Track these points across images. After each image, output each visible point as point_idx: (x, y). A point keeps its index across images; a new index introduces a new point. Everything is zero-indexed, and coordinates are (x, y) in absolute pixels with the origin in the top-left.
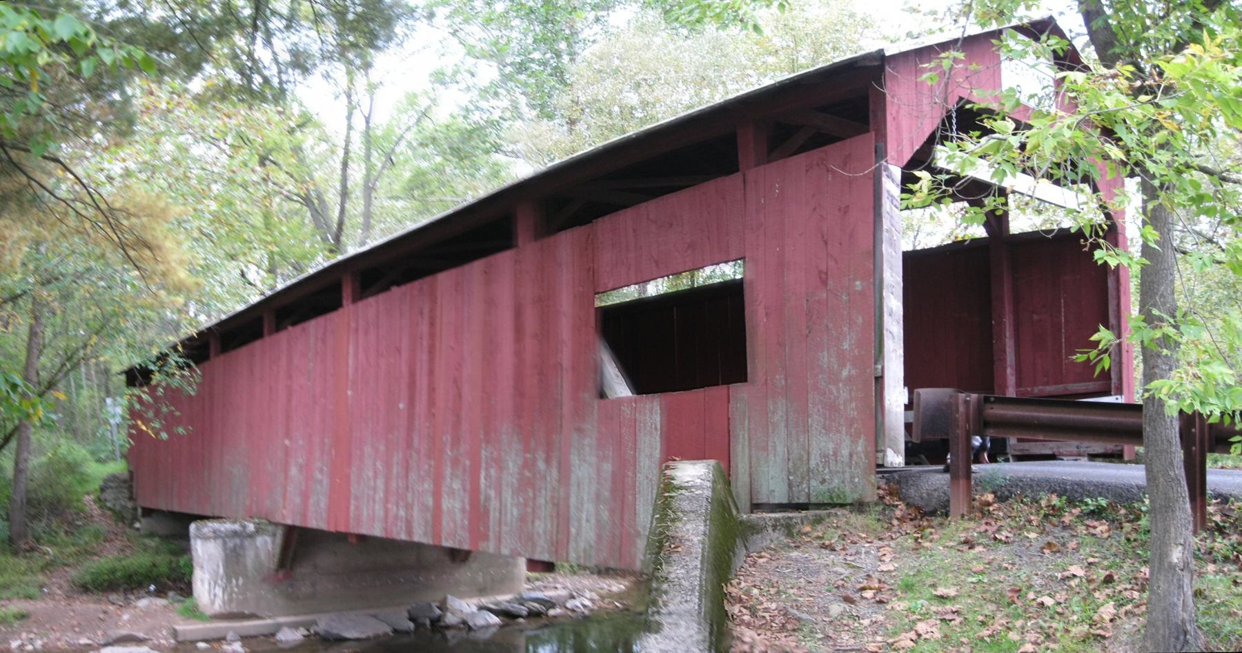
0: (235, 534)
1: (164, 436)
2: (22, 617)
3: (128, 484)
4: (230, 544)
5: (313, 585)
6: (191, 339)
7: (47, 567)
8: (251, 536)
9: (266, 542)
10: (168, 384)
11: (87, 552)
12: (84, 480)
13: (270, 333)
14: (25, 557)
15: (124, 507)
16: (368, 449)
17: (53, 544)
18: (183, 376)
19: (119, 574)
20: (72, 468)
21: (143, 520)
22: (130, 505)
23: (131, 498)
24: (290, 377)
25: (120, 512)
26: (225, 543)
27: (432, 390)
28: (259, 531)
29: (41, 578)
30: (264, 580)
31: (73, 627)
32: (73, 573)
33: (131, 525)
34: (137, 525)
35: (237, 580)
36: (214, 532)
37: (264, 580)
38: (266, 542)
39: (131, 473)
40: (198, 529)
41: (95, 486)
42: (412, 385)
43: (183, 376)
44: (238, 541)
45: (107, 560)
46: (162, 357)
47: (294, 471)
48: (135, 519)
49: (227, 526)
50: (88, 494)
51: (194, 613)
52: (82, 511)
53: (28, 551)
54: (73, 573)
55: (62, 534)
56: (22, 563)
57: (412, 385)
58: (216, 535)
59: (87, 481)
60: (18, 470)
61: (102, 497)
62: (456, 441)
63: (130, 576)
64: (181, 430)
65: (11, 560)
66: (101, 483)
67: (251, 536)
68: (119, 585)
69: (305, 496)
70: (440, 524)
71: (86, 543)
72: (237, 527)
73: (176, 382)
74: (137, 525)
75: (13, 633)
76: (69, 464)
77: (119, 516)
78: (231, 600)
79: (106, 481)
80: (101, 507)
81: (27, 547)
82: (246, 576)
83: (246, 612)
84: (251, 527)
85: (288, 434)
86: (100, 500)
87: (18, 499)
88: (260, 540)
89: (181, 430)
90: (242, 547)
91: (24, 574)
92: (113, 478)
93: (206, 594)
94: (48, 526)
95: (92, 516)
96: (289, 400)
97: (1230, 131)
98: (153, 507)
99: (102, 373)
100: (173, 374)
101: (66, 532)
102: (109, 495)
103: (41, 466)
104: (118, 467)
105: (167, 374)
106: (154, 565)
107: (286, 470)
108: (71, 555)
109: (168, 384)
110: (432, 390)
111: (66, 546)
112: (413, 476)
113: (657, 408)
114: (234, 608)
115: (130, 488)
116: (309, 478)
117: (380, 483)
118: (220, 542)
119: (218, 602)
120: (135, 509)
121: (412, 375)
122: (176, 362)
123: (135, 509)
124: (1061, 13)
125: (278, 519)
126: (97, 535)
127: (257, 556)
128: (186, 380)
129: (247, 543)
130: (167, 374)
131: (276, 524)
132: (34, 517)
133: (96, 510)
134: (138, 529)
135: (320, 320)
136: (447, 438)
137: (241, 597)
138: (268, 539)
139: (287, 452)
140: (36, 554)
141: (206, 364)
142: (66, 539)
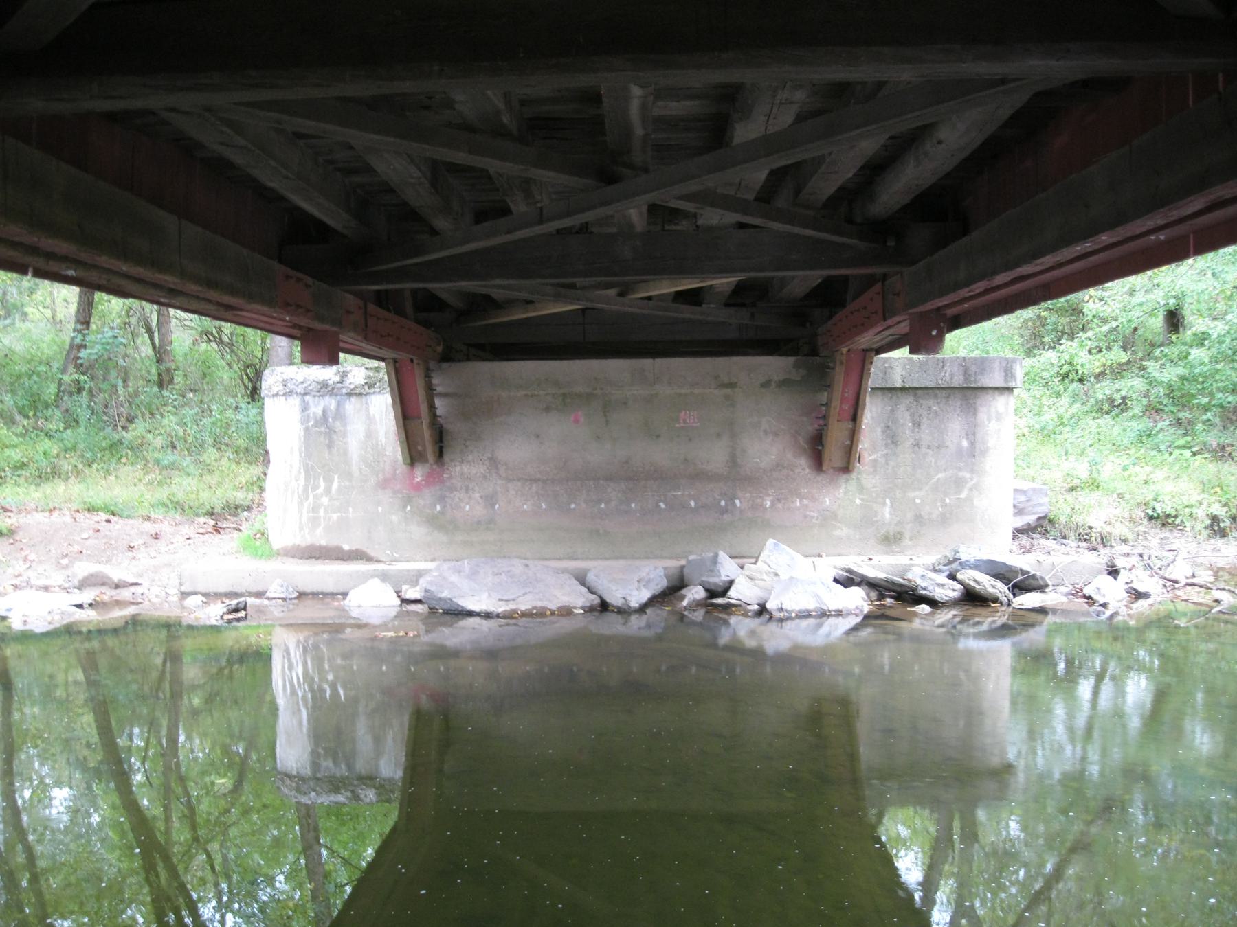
4: (317, 407)
5: (490, 500)
26: (305, 408)
30: (384, 484)
35: (329, 481)
37: (384, 484)
44: (331, 402)
51: (260, 543)
70: (1090, 256)
78: (314, 521)
82: (348, 475)
83: (346, 547)
90: (340, 414)
97: (125, 594)
99: (15, 306)
113: (384, 773)
114: (321, 539)
124: (938, 924)
129: (351, 406)
137: (335, 516)
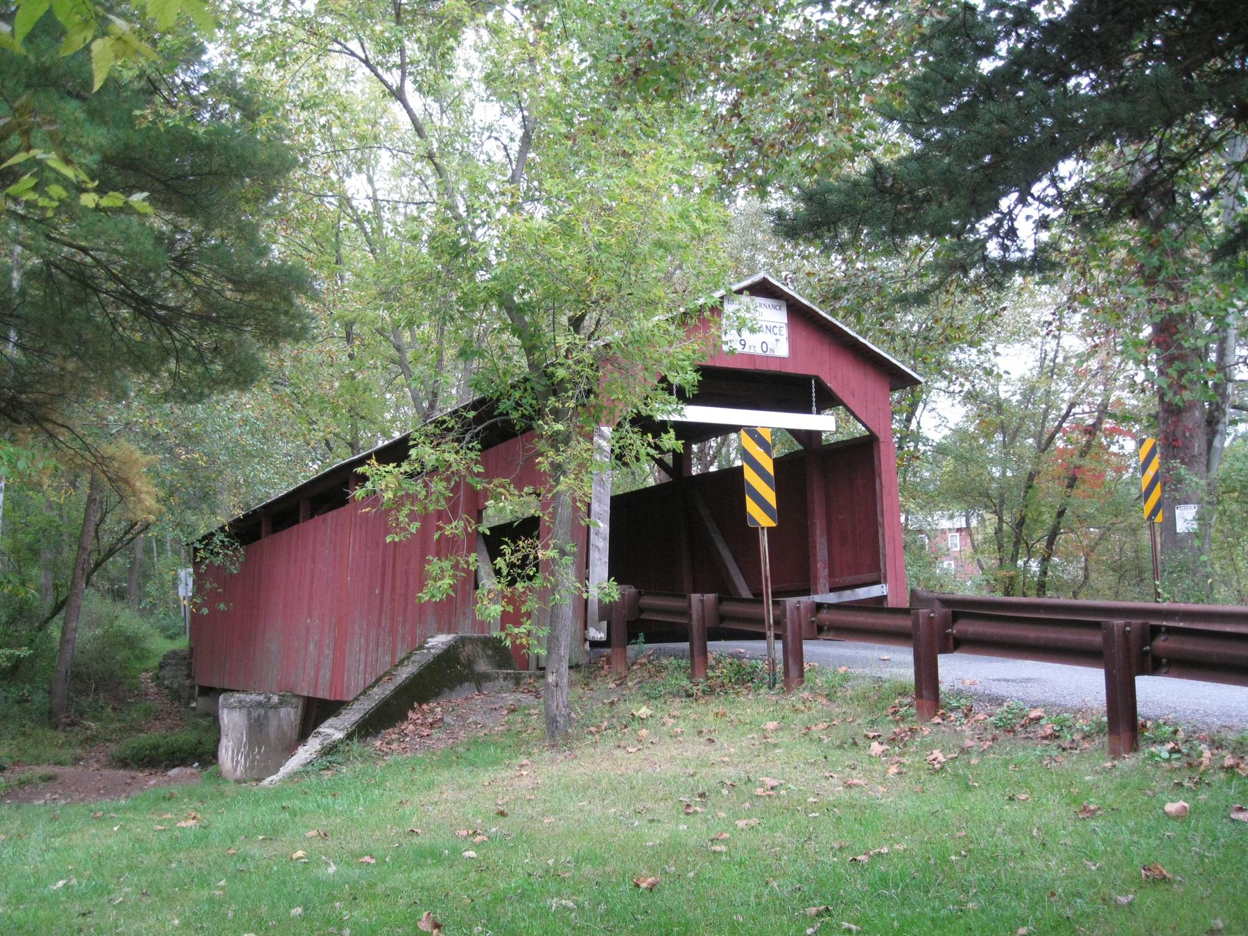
0: (260, 704)
1: (205, 611)
2: (49, 779)
3: (186, 661)
4: (255, 714)
6: (238, 520)
7: (89, 741)
8: (275, 707)
9: (289, 714)
10: (211, 562)
11: (132, 727)
12: (143, 656)
13: (305, 519)
14: (64, 731)
15: (181, 685)
16: (357, 628)
17: (95, 719)
18: (226, 555)
19: (161, 750)
20: (131, 642)
21: (200, 699)
22: (187, 683)
23: (189, 676)
24: (314, 562)
25: (177, 691)
26: (249, 713)
27: (394, 579)
28: (282, 703)
29: (79, 751)
31: (99, 789)
32: (113, 748)
33: (187, 705)
34: (194, 705)
35: (260, 749)
36: (240, 702)
38: (289, 714)
39: (191, 649)
40: (225, 699)
41: (154, 663)
42: (383, 576)
43: (226, 555)
44: (262, 712)
45: (154, 735)
46: (209, 537)
47: (311, 647)
48: (192, 698)
49: (254, 697)
50: (147, 671)
52: (137, 688)
53: (69, 725)
54: (113, 748)
55: (109, 710)
56: (61, 737)
57: (383, 576)
58: (241, 705)
59: (148, 658)
60: (64, 640)
61: (161, 674)
62: (404, 622)
63: (173, 753)
64: (222, 606)
65: (49, 733)
66: (160, 659)
67: (275, 707)
68: (161, 762)
69: (318, 670)
71: (133, 719)
72: (262, 698)
73: (218, 561)
74: (194, 705)
75: (39, 793)
76: (127, 638)
77: (176, 695)
78: (252, 767)
79: (166, 657)
80: (157, 686)
81: (68, 721)
84: (275, 699)
85: (310, 614)
86: (158, 678)
87: (63, 670)
88: (283, 711)
89: (222, 606)
90: (266, 716)
91: (62, 746)
92: (174, 654)
93: (229, 761)
94: (96, 701)
95: (146, 695)
96: (312, 583)
98: (207, 684)
100: (218, 554)
101: (114, 709)
102: (167, 672)
103: (96, 638)
104: (182, 644)
105: (212, 552)
106: (200, 743)
107: (306, 647)
108: (114, 731)
109: (211, 562)
110: (394, 579)
111: (112, 721)
112: (380, 649)
115: (190, 664)
116: (320, 653)
117: (362, 656)
118: (245, 711)
119: (240, 769)
120: (192, 687)
121: (384, 563)
122: (222, 541)
123: (192, 687)
125: (298, 692)
126: (147, 712)
127: (280, 726)
128: (231, 560)
129: (271, 713)
130: (212, 552)
131: (299, 696)
132: (80, 692)
133: (152, 689)
134: (194, 709)
135: (334, 512)
136: (400, 619)
138: (292, 711)
139: (308, 629)
140: (77, 729)
141: (253, 546)
142: (112, 715)
